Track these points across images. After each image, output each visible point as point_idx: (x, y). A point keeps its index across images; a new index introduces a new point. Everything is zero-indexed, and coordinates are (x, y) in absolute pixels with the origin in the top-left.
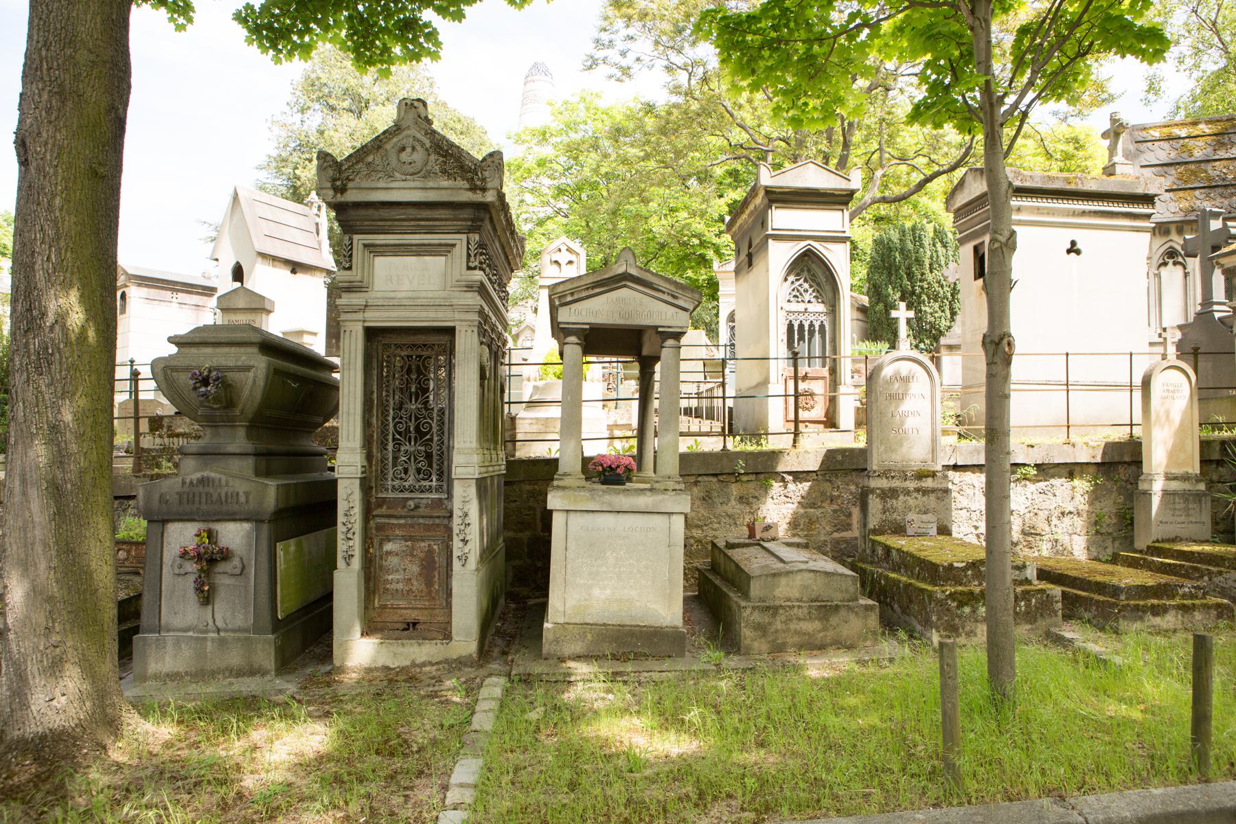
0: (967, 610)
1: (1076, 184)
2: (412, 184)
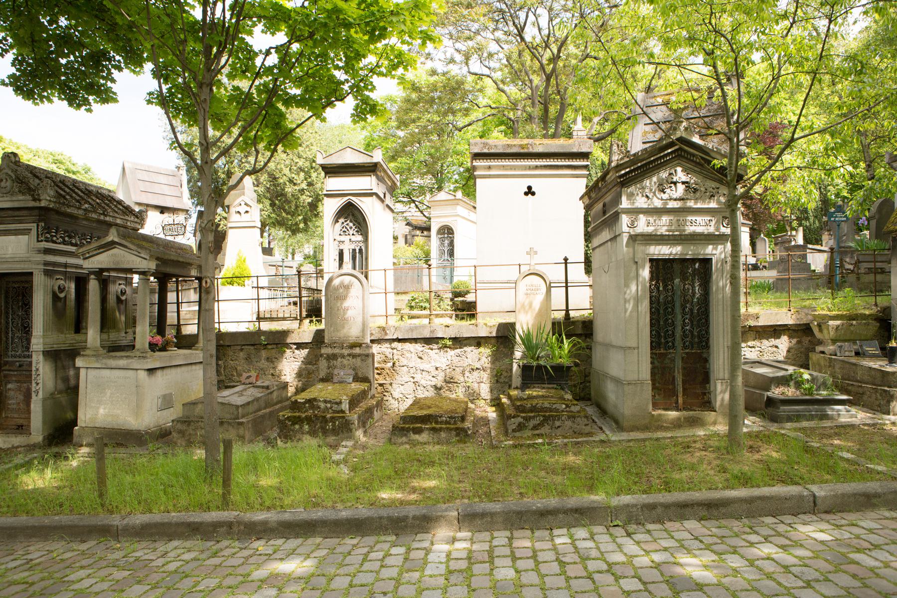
0: (297, 427)
1: (528, 148)
2: (6, 199)
